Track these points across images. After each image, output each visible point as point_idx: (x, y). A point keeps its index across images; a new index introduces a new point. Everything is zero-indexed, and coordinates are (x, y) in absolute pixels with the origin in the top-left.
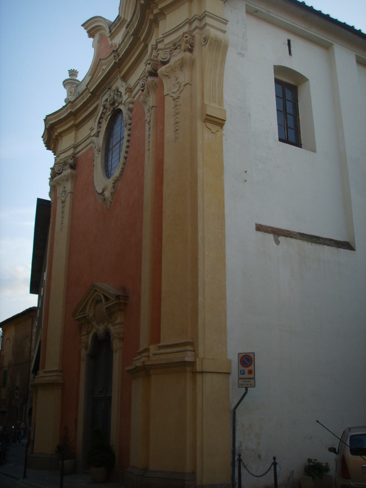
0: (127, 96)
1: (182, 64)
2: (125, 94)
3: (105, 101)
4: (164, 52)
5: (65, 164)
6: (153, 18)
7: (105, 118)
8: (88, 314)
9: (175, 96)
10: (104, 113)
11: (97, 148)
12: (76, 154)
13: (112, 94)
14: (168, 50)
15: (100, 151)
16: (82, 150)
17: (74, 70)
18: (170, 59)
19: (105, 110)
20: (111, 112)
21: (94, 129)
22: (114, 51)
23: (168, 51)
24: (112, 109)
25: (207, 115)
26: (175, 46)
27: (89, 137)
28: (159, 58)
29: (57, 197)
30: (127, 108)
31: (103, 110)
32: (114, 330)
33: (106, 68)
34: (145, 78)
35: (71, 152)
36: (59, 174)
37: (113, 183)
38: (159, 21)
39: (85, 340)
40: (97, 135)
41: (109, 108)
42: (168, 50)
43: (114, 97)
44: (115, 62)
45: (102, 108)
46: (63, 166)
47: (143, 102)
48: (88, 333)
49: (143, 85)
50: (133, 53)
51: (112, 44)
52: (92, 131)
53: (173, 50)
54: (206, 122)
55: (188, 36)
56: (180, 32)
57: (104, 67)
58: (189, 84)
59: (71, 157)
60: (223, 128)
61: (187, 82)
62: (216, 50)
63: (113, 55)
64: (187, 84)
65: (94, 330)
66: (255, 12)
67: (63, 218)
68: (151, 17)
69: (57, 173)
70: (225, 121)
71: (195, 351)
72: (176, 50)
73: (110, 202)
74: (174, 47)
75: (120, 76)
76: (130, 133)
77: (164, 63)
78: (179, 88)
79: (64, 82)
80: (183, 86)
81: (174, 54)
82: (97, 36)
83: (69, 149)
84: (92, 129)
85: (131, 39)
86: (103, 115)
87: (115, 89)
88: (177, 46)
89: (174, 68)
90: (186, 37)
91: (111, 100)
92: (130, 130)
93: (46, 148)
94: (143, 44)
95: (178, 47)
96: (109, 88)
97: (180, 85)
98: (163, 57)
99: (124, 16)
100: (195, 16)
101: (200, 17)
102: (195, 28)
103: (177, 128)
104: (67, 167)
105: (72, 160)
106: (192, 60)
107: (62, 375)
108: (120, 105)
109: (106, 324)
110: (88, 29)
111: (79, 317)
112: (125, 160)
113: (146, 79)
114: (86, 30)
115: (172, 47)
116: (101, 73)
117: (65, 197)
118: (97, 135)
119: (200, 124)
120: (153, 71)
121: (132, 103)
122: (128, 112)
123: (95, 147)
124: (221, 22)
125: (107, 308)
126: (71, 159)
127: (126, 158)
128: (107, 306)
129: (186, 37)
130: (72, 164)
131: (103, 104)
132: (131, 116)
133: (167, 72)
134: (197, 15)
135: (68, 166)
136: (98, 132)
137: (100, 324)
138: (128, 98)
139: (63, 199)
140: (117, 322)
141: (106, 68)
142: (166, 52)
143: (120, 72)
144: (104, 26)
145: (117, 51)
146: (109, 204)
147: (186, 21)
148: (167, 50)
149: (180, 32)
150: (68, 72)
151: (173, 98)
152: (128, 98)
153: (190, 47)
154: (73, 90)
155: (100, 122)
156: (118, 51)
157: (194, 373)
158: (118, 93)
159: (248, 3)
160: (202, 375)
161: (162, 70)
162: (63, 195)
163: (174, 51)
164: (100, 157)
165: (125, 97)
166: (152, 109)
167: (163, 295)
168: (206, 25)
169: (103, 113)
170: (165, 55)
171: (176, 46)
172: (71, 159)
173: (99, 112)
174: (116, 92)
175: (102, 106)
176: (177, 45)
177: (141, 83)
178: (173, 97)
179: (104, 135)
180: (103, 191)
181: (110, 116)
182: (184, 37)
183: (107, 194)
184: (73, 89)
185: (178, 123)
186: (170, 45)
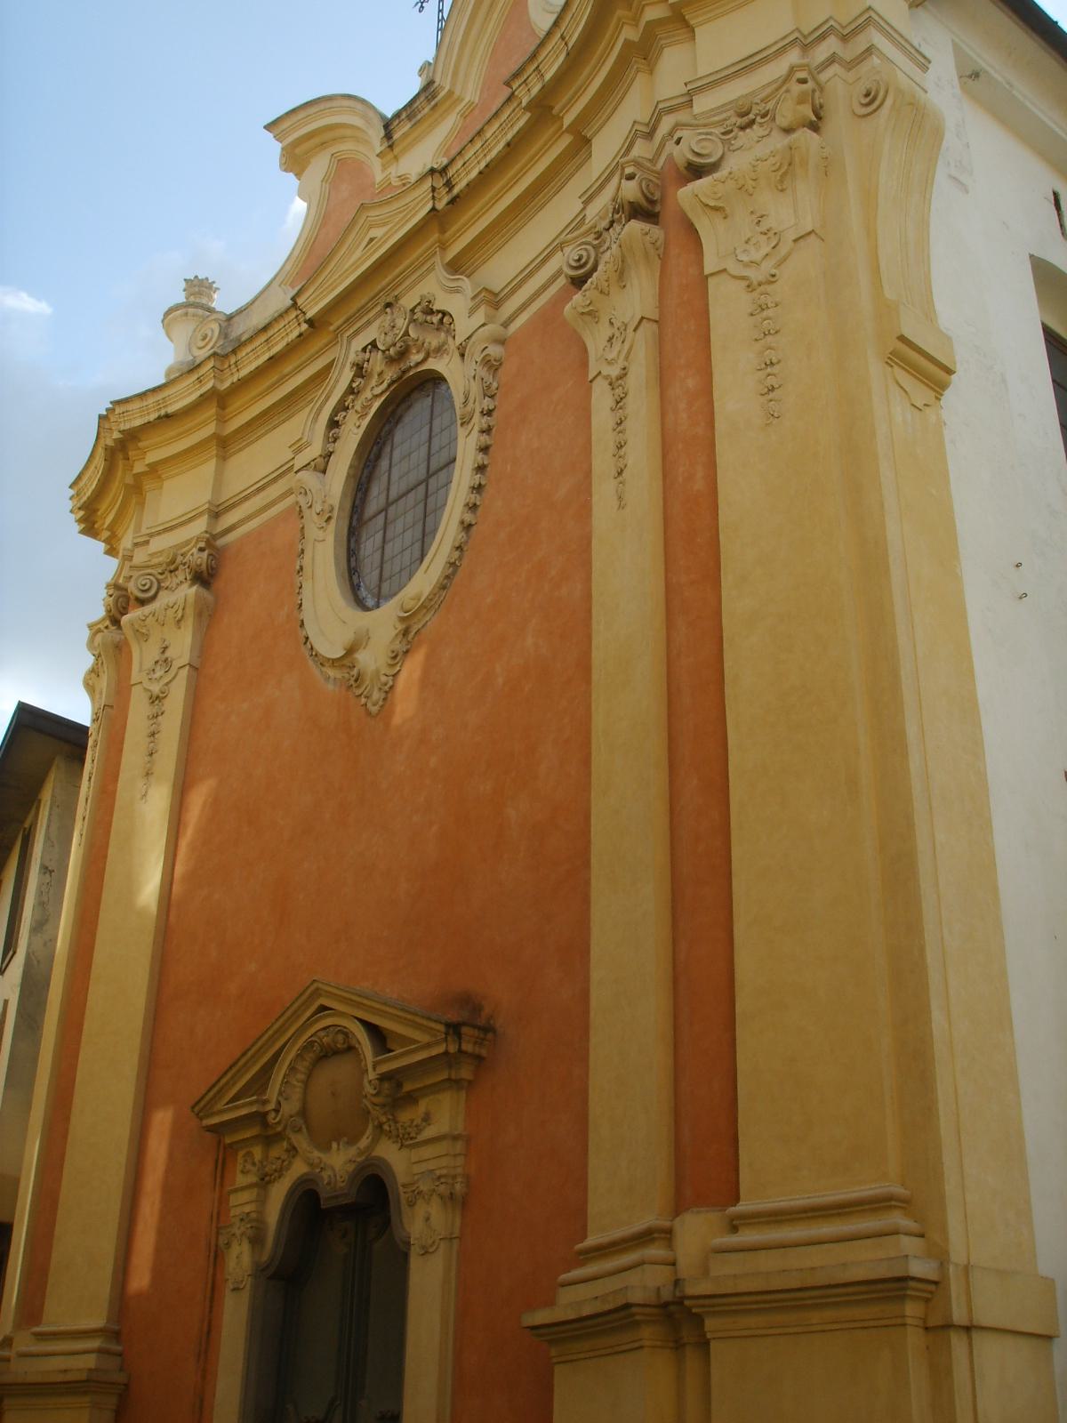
0: (480, 316)
1: (786, 172)
2: (472, 312)
3: (364, 350)
4: (700, 134)
5: (172, 567)
6: (636, 39)
7: (358, 407)
8: (279, 1103)
9: (755, 275)
11: (318, 508)
12: (215, 537)
13: (401, 323)
14: (717, 131)
15: (329, 518)
16: (243, 523)
17: (207, 279)
18: (722, 158)
19: (359, 380)
20: (389, 386)
21: (308, 444)
22: (432, 171)
23: (717, 132)
24: (390, 374)
25: (902, 339)
26: (747, 117)
27: (286, 471)
28: (681, 154)
29: (132, 683)
30: (479, 360)
31: (352, 381)
32: (398, 1161)
33: (387, 236)
34: (590, 238)
35: (199, 527)
36: (142, 602)
37: (402, 619)
38: (662, 48)
39: (247, 1209)
40: (322, 466)
41: (380, 374)
42: (717, 131)
43: (406, 333)
44: (433, 209)
45: (348, 374)
46: (160, 577)
47: (583, 313)
48: (265, 1182)
49: (583, 260)
50: (492, 198)
51: (387, 178)
52: (299, 451)
53: (736, 130)
54: (896, 367)
55: (809, 80)
56: (776, 70)
57: (377, 233)
58: (816, 234)
59: (202, 545)
60: (942, 398)
61: (810, 229)
62: (909, 135)
63: (428, 184)
64: (810, 233)
65: (298, 1169)
66: (970, 76)
67: (151, 754)
68: (630, 33)
69: (137, 599)
70: (950, 372)
71: (931, 1234)
72: (748, 130)
73: (386, 688)
74: (740, 121)
75: (442, 258)
76: (489, 443)
77: (696, 171)
78: (774, 248)
79: (167, 314)
80: (790, 243)
81: (737, 143)
82: (320, 165)
83: (191, 520)
84: (298, 448)
85: (521, 123)
86: (351, 397)
87: (415, 307)
88: (756, 115)
89: (751, 182)
90: (803, 81)
91: (394, 345)
92: (487, 431)
93: (77, 527)
94: (566, 140)
95: (759, 119)
96: (389, 305)
97: (780, 240)
98: (696, 150)
99: (453, 84)
100: (827, 21)
101: (843, 27)
102: (827, 60)
103: (771, 381)
104: (176, 581)
105: (206, 552)
106: (827, 158)
107: (119, 1348)
108: (430, 359)
109: (364, 1142)
110: (290, 139)
111: (226, 1117)
112: (463, 534)
113: (596, 242)
114: (281, 142)
115: (733, 120)
116: (358, 253)
117: (166, 680)
118: (322, 466)
119: (875, 369)
120: (644, 203)
121: (501, 342)
122: (483, 372)
123: (311, 507)
124: (913, 60)
125: (383, 1078)
126: (201, 550)
127: (467, 527)
128: (384, 1068)
129: (803, 81)
130: (204, 567)
131: (352, 357)
132: (495, 385)
133: (719, 195)
134: (835, 21)
135: (181, 575)
136: (328, 456)
137: (334, 1145)
138: (483, 325)
139: (156, 688)
140: (429, 1132)
141: (387, 233)
142: (707, 134)
143: (444, 247)
144: (355, 124)
145: (444, 170)
146: (376, 695)
147: (791, 38)
148: (713, 130)
149: (776, 70)
150: (183, 285)
151: (744, 283)
152: (483, 325)
153: (814, 118)
154: (213, 331)
155: (338, 422)
156: (450, 173)
157: (939, 1329)
158: (429, 318)
159: (957, 40)
160: (970, 1339)
161: (687, 195)
162: (158, 674)
163: (741, 133)
164: (330, 539)
165: (464, 325)
166: (639, 331)
167: (743, 1004)
168: (871, 54)
169: (351, 391)
170: (704, 143)
171: (751, 116)
172: (201, 550)
173: (334, 387)
174: (419, 315)
175: (348, 365)
176: (755, 111)
177: (571, 253)
178: (743, 278)
179: (351, 467)
180: (351, 651)
181: (383, 399)
182: (794, 79)
183: (371, 660)
184: (216, 327)
185: (779, 362)
186: (728, 114)
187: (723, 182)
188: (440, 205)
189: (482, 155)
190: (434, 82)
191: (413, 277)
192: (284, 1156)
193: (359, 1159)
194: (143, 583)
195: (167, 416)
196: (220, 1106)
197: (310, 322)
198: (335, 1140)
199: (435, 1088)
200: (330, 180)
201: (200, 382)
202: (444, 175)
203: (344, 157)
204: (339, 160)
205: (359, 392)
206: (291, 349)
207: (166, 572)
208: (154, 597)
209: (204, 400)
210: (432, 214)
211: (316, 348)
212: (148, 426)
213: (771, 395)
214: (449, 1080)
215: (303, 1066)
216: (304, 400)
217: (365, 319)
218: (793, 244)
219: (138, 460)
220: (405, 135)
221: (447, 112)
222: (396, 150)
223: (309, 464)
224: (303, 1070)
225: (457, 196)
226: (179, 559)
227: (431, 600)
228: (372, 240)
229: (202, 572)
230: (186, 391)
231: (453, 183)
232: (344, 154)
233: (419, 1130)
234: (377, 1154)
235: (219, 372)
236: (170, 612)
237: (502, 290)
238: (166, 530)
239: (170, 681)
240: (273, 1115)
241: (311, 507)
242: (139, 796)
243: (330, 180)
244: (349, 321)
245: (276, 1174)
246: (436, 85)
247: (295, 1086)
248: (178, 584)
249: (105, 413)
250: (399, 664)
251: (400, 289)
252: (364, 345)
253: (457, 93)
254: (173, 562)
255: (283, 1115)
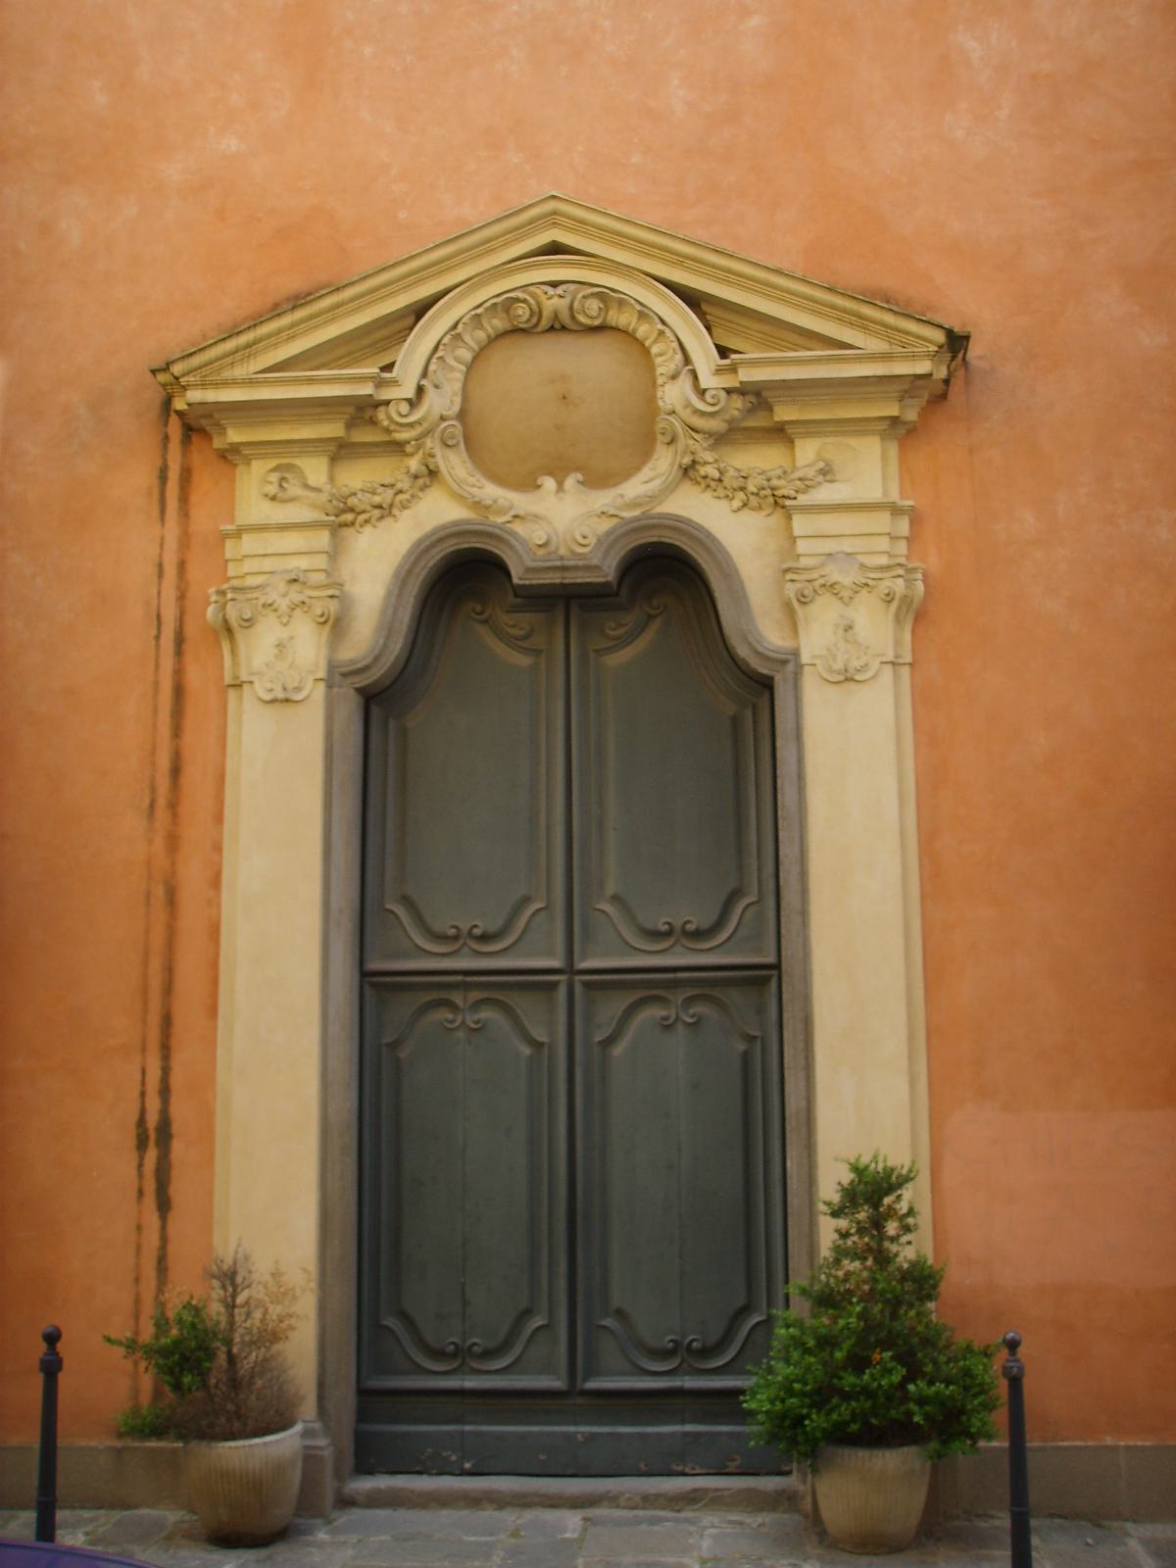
8: (420, 390)
192: (405, 483)
193: (627, 514)
196: (239, 372)
198: (550, 474)
199: (858, 427)
214: (894, 421)
215: (474, 338)
224: (472, 344)
233: (807, 485)
234: (302, 466)
240: (404, 408)
245: (377, 513)
247: (452, 369)
255: (428, 412)
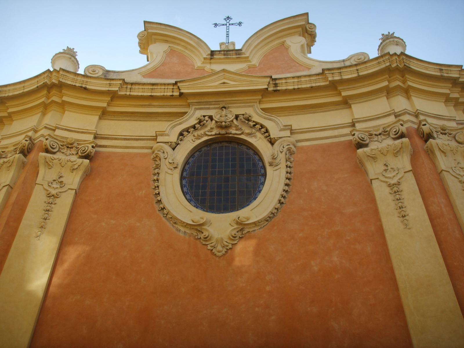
5: (70, 146)
9: (392, 182)
10: (196, 128)
31: (196, 124)
33: (234, 86)
38: (398, 95)
44: (267, 89)
86: (193, 129)
103: (403, 213)
115: (440, 130)
169: (194, 127)
171: (446, 132)
178: (47, 191)
187: (446, 146)
188: (270, 89)
189: (297, 84)
190: (242, 50)
191: (240, 105)
194: (53, 144)
195: (85, 89)
197: (181, 94)
200: (166, 53)
201: (111, 85)
202: (274, 81)
203: (175, 50)
204: (171, 49)
205: (197, 129)
206: (164, 98)
207: (65, 146)
208: (54, 153)
209: (108, 92)
210: (265, 90)
211: (176, 104)
212: (73, 87)
213: (47, 212)
216: (157, 118)
217: (208, 106)
218: (403, 173)
219: (55, 95)
220: (220, 59)
221: (241, 62)
222: (212, 61)
223: (168, 142)
225: (279, 90)
226: (75, 145)
227: (260, 222)
228: (224, 83)
229: (90, 156)
230: (101, 85)
231: (278, 85)
232: (175, 49)
235: (121, 86)
236: (70, 164)
237: (296, 130)
238: (66, 130)
239: (63, 192)
241: (166, 159)
242: (34, 235)
243: (166, 53)
244: (199, 103)
246: (242, 52)
248: (70, 154)
249: (58, 69)
250: (237, 241)
251: (231, 105)
252: (206, 115)
253: (250, 58)
254: (72, 144)
